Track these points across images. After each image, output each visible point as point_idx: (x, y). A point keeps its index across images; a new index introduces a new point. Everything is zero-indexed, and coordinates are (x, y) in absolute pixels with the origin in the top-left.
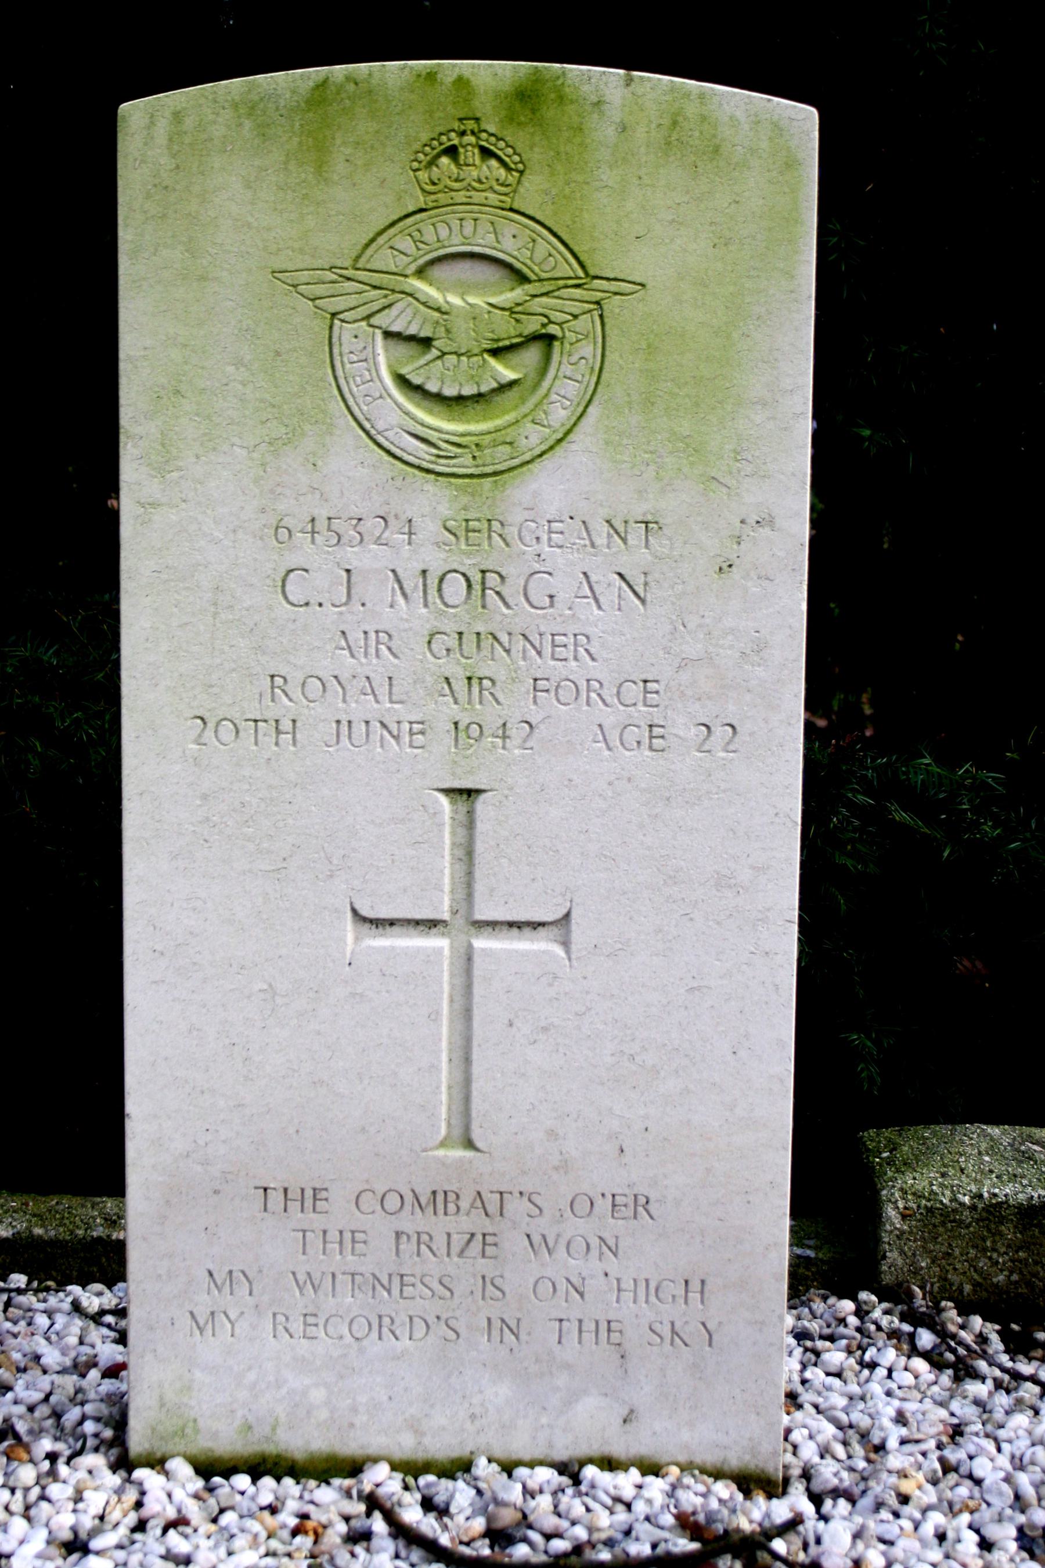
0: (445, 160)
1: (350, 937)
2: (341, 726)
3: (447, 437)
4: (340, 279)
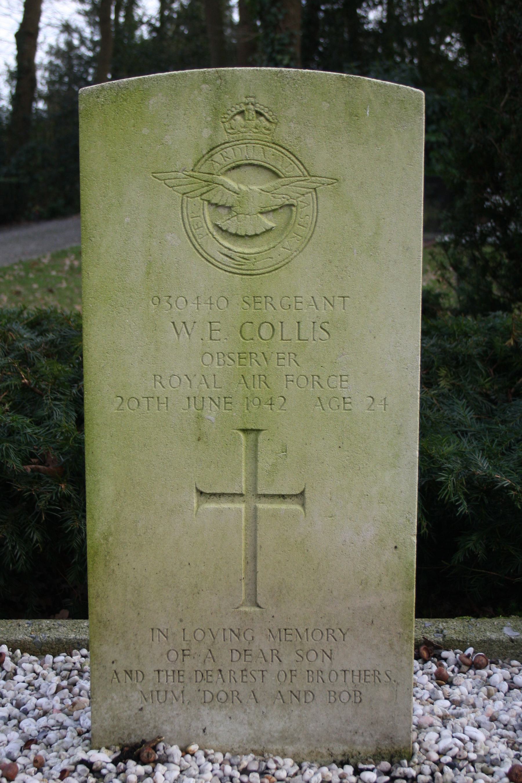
0: (238, 118)
1: (195, 501)
4: (187, 177)
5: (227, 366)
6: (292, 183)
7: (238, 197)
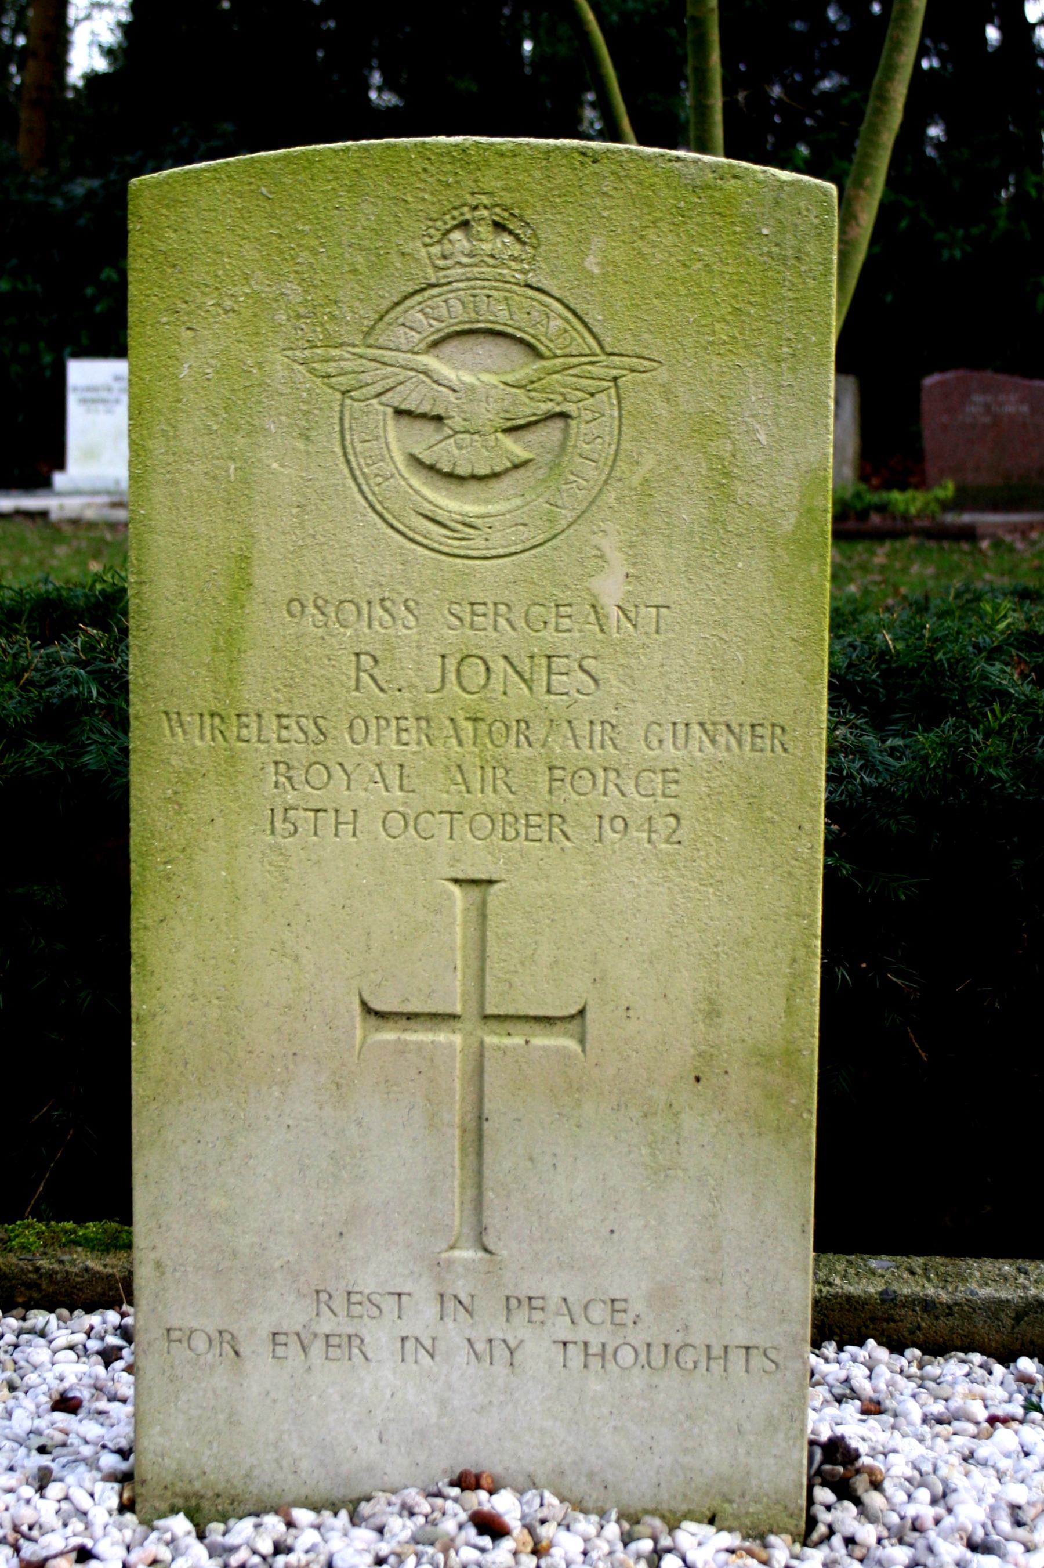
0: (456, 235)
1: (359, 1034)
2: (603, 821)
3: (459, 518)
5: (312, 745)
6: (571, 368)
7: (457, 399)
